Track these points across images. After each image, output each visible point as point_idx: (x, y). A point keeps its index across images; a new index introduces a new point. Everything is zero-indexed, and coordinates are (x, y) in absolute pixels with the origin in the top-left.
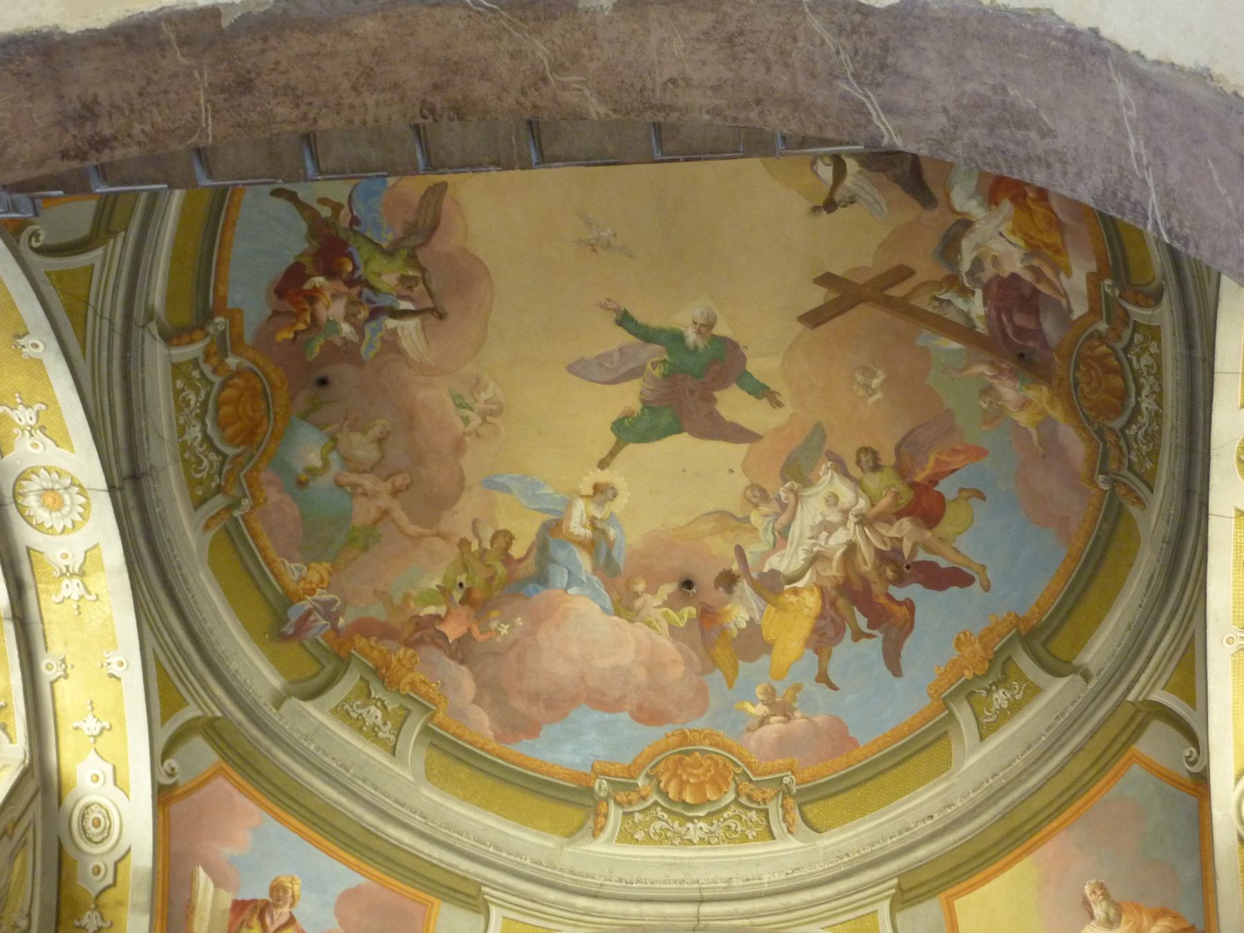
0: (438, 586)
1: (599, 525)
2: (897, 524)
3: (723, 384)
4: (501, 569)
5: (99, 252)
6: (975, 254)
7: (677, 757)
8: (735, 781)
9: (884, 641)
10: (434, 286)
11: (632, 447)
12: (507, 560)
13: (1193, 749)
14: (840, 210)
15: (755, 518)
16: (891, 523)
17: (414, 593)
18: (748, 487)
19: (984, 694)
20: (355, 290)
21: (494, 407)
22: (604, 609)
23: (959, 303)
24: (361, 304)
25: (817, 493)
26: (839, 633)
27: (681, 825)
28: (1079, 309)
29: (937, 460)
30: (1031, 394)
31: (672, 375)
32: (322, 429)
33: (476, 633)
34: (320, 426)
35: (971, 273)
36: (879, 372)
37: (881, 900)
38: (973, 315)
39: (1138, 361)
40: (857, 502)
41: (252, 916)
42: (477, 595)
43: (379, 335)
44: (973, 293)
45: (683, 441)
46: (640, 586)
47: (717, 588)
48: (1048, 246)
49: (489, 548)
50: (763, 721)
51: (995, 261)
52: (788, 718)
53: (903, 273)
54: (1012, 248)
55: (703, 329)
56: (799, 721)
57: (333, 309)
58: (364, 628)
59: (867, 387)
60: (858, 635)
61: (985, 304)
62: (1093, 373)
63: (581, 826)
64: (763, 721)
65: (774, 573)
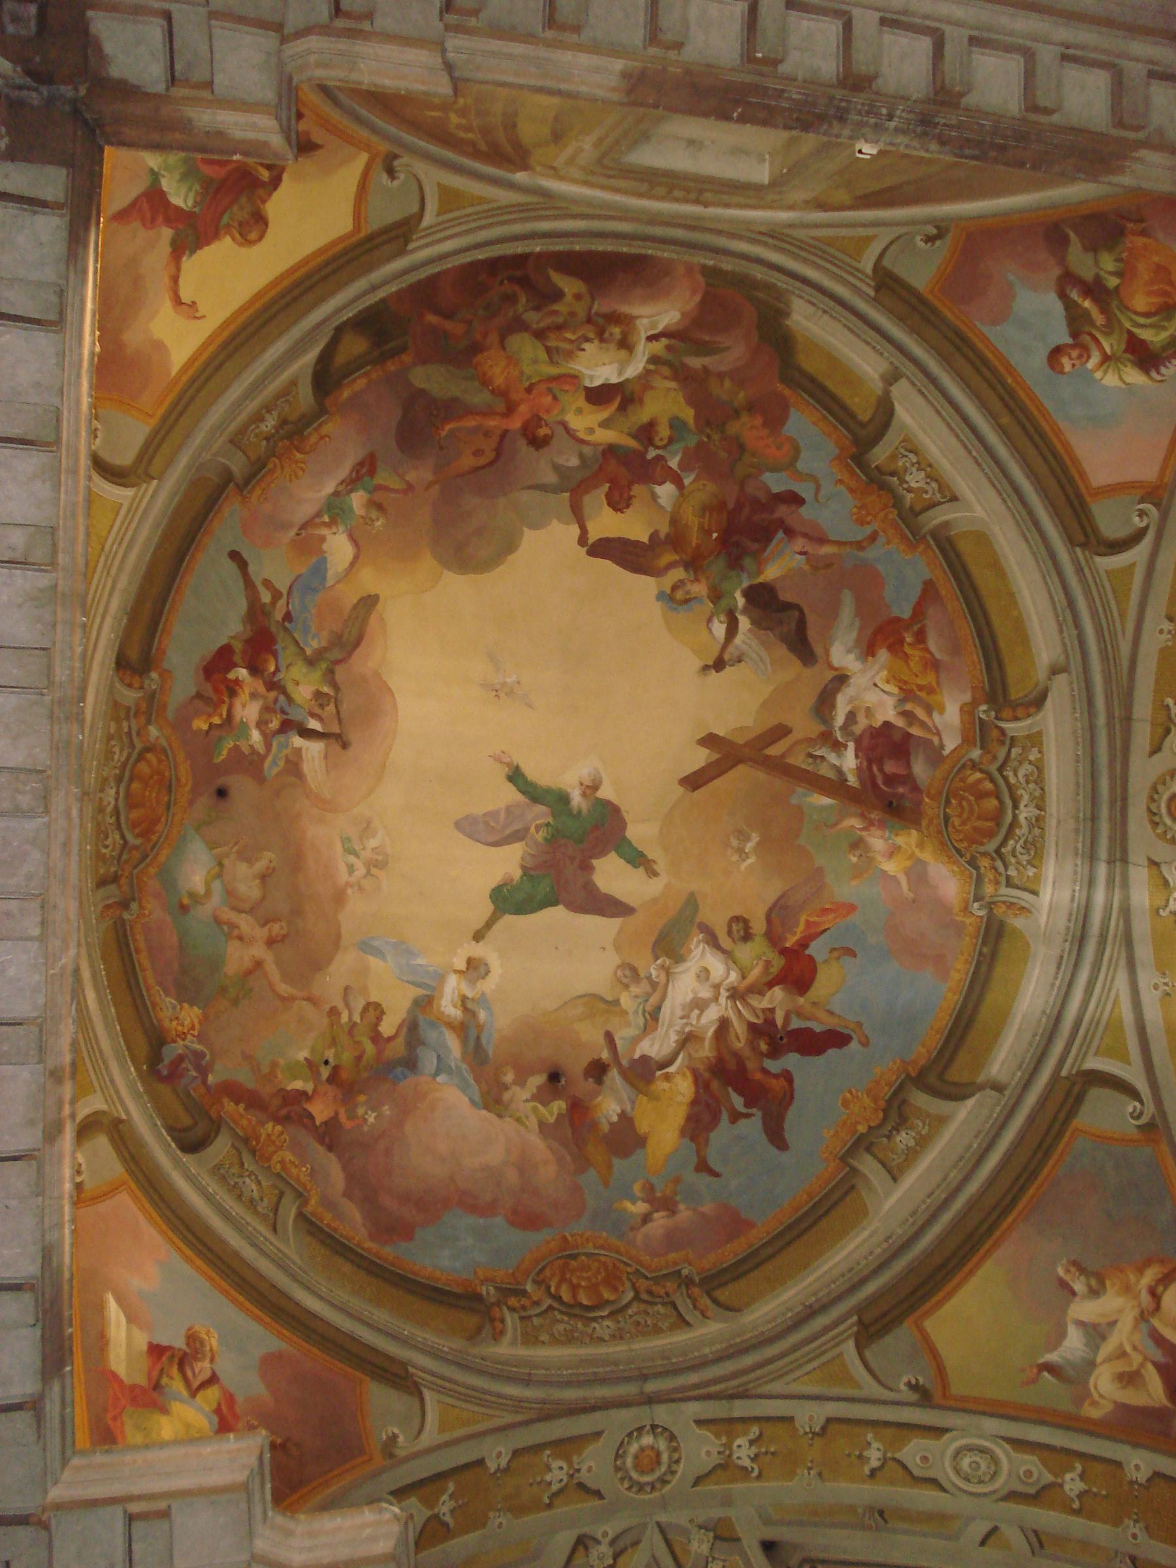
0: (306, 1059)
1: (469, 1006)
2: (769, 994)
3: (602, 853)
4: (370, 1048)
5: (129, 492)
6: (849, 708)
7: (561, 1262)
8: (630, 1280)
9: (764, 1118)
10: (344, 707)
11: (508, 919)
12: (376, 1038)
13: (1137, 1104)
14: (728, 669)
15: (626, 1001)
16: (761, 993)
17: (282, 1061)
18: (619, 967)
19: (885, 1140)
20: (273, 694)
21: (380, 858)
22: (472, 1101)
23: (832, 758)
24: (275, 712)
25: (688, 970)
26: (715, 1119)
27: (585, 1325)
28: (951, 743)
29: (807, 922)
30: (900, 840)
31: (555, 839)
32: (211, 849)
33: (343, 1117)
34: (212, 845)
35: (845, 728)
36: (754, 834)
37: (844, 1341)
38: (845, 769)
39: (1016, 775)
40: (728, 973)
41: (171, 1364)
42: (344, 1075)
43: (285, 752)
44: (846, 746)
45: (558, 913)
46: (509, 1077)
47: (586, 1080)
48: (921, 688)
49: (359, 1021)
50: (646, 1219)
51: (869, 712)
52: (673, 1212)
53: (780, 732)
54: (885, 697)
55: (588, 792)
56: (684, 1213)
57: (248, 710)
58: (232, 1090)
59: (740, 851)
60: (735, 1117)
61: (857, 756)
62: (964, 803)
63: (479, 1330)
64: (646, 1219)
65: (645, 1059)
